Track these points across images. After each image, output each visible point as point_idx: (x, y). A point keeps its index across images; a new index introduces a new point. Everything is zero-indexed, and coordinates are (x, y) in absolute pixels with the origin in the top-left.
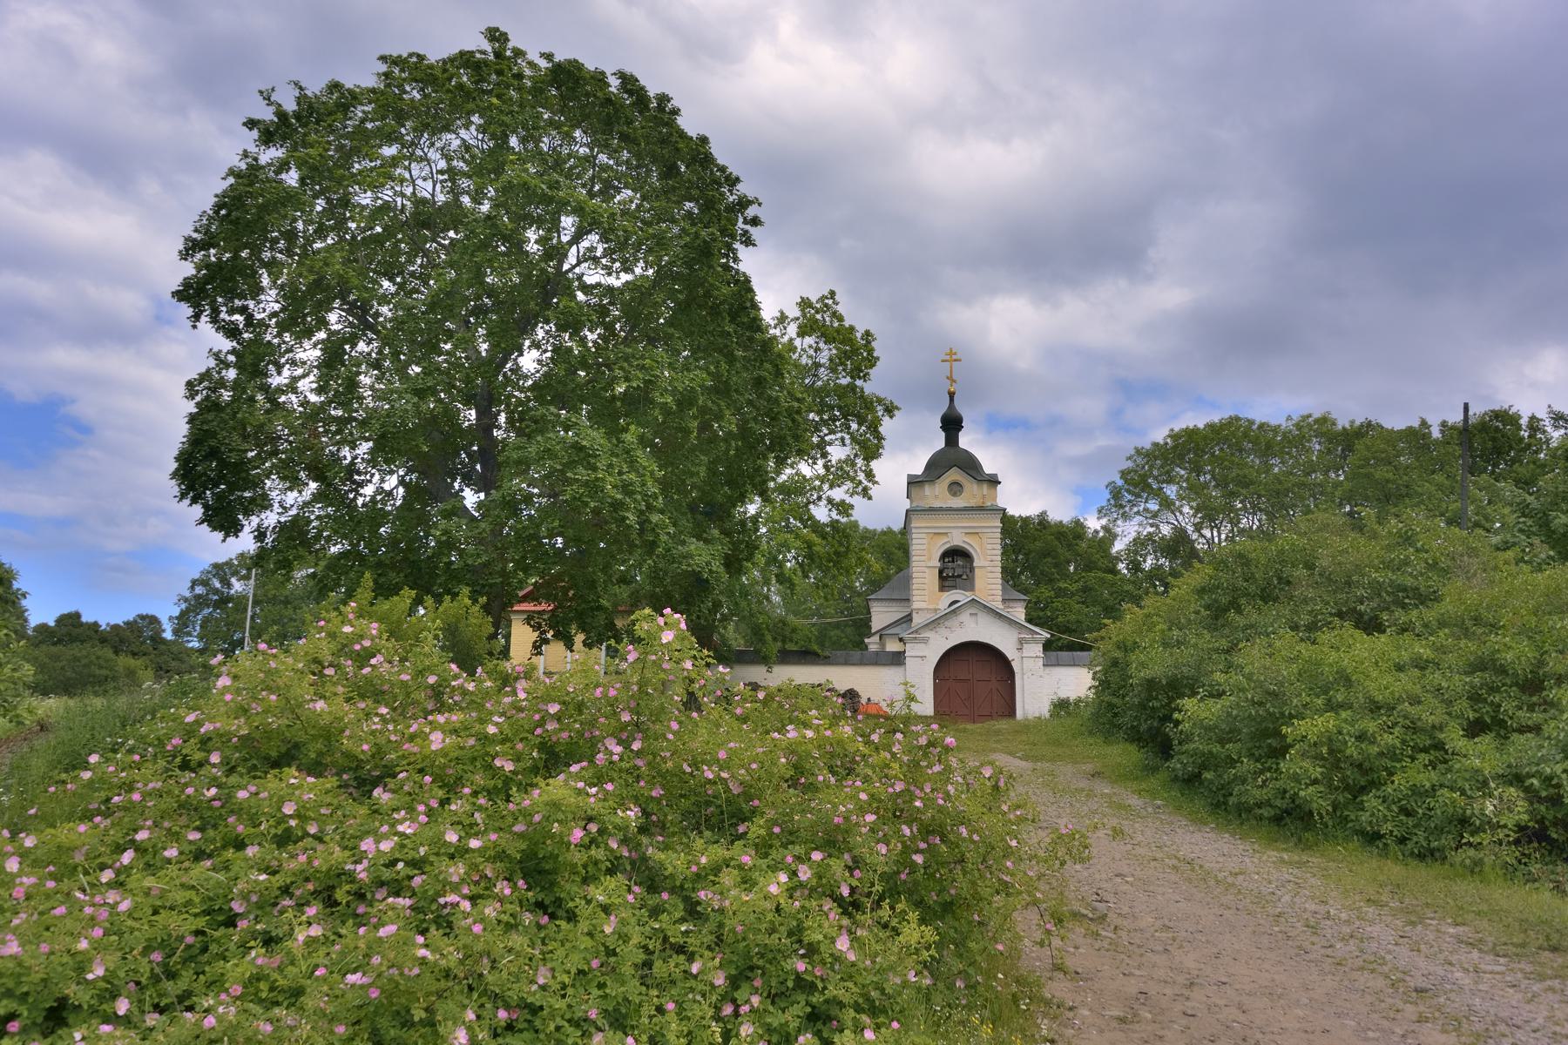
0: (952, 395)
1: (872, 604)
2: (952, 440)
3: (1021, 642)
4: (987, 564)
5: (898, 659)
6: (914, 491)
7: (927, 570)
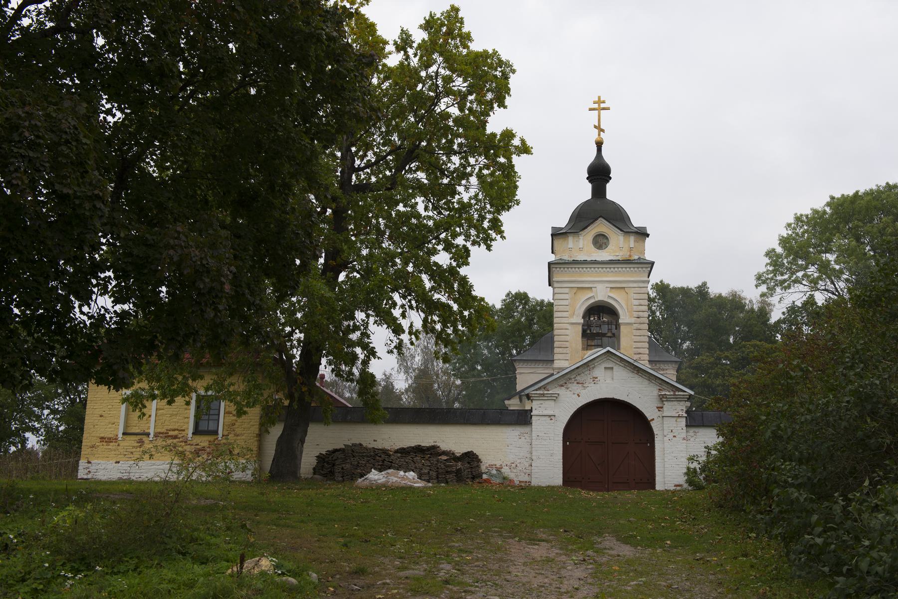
0: (599, 145)
1: (517, 365)
2: (599, 191)
3: (662, 398)
4: (633, 320)
5: (523, 419)
6: (558, 243)
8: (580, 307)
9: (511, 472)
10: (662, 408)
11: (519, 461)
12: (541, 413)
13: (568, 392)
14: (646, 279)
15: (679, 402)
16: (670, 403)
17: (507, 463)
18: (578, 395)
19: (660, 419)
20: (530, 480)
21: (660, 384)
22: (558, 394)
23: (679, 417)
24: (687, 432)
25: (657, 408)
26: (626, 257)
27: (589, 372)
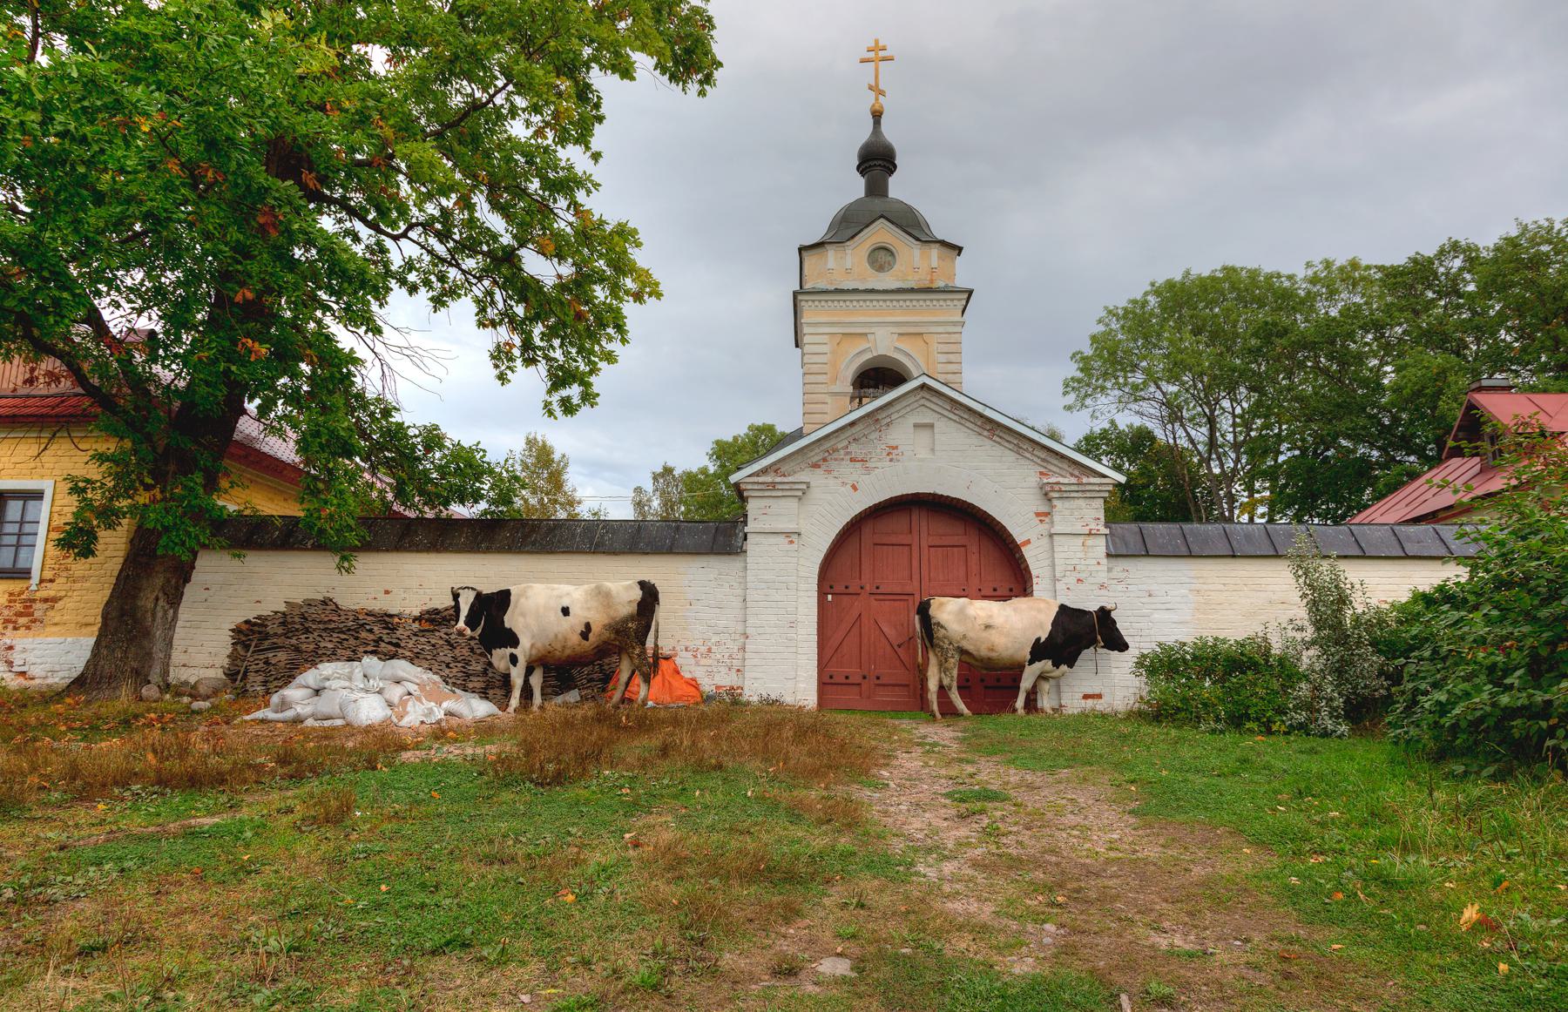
0: (877, 116)
2: (876, 188)
7: (828, 399)
8: (852, 361)
9: (697, 664)
10: (1047, 514)
11: (715, 639)
12: (767, 528)
13: (831, 481)
14: (958, 318)
15: (1087, 501)
16: (1067, 504)
17: (688, 644)
18: (854, 488)
19: (1046, 540)
20: (740, 684)
21: (1044, 460)
22: (808, 484)
23: (1090, 534)
24: (1110, 570)
25: (1038, 514)
26: (927, 284)
27: (877, 434)
